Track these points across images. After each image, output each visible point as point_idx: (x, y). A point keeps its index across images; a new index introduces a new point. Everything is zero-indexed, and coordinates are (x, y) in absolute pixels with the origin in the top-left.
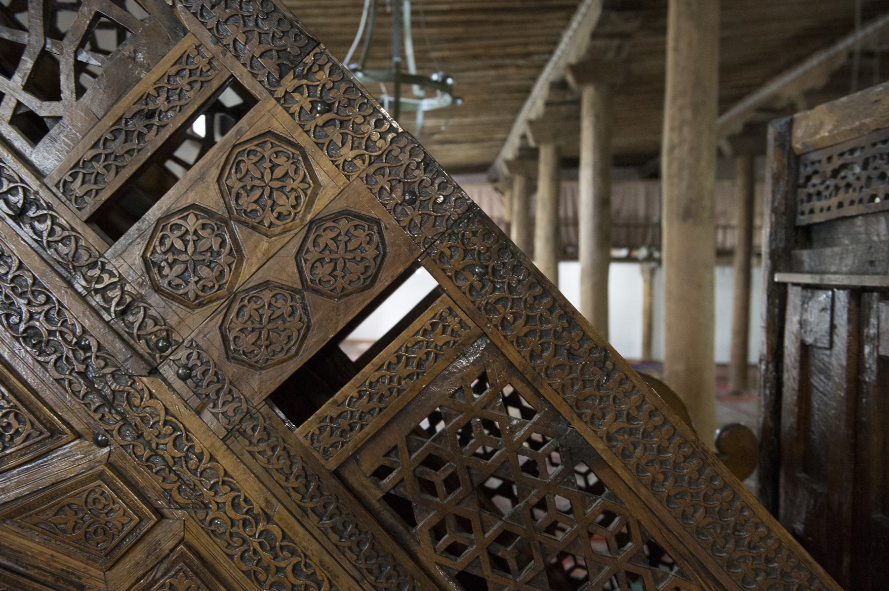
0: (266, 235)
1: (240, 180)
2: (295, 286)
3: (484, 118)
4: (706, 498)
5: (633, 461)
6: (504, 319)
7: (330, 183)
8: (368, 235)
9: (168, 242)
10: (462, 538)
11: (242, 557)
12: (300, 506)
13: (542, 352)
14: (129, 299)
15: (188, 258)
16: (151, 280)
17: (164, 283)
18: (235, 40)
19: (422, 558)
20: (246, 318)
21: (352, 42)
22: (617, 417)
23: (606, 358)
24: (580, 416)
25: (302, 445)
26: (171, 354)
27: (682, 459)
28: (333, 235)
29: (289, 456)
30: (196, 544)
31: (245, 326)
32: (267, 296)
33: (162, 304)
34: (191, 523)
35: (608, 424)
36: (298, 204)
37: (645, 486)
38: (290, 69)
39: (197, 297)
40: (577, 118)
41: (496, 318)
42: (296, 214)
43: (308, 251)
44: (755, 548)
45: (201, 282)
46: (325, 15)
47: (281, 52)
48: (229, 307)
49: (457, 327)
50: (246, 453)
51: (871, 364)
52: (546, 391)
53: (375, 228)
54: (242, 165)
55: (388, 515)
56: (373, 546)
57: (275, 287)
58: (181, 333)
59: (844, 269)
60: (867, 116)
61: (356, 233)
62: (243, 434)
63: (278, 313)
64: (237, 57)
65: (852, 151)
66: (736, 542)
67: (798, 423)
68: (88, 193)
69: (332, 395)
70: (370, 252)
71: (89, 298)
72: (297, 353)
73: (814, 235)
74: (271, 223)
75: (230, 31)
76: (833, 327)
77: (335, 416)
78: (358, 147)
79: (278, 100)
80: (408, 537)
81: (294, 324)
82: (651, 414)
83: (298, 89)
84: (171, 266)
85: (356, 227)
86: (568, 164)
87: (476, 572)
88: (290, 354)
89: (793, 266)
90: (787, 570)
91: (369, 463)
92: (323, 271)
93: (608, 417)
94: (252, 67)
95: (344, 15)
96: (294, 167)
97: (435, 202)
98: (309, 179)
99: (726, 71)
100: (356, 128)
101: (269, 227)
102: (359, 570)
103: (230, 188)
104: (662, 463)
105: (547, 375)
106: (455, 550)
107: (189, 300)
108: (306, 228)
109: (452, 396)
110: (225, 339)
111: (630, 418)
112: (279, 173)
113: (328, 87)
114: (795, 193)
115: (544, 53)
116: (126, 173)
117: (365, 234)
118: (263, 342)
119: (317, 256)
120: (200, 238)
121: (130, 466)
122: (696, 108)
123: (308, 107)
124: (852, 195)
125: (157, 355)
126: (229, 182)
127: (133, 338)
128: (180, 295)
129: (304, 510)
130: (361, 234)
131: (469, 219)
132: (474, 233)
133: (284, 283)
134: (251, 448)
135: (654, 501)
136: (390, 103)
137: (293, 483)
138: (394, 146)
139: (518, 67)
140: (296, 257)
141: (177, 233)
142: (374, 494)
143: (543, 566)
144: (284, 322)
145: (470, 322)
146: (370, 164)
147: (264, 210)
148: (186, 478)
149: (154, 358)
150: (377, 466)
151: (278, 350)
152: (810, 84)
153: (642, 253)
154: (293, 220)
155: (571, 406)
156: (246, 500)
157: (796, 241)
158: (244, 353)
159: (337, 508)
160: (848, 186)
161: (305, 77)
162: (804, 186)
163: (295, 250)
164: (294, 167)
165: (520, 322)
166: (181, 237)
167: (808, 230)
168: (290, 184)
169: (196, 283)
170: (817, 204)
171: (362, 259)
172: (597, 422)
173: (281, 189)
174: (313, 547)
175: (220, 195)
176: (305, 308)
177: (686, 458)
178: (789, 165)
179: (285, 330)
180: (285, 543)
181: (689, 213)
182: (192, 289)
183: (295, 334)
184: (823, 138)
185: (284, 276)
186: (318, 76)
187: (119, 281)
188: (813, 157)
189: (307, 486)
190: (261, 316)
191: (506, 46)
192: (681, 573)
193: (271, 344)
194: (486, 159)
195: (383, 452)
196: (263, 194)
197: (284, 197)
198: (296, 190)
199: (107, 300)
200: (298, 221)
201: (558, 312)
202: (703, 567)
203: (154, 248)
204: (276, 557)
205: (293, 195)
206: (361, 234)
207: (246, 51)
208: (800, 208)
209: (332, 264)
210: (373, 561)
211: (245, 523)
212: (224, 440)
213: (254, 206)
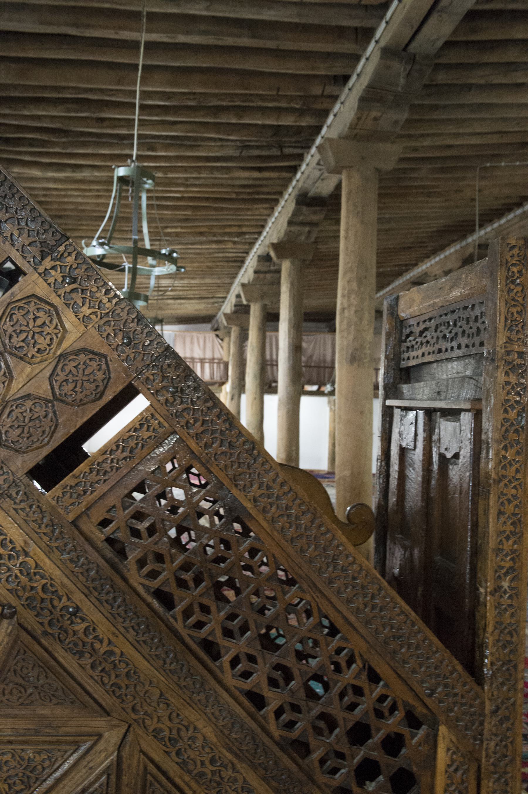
0: (29, 363)
1: (12, 326)
3: (208, 281)
5: (270, 515)
6: (188, 422)
7: (74, 331)
10: (157, 566)
11: (7, 580)
12: (48, 546)
13: (212, 443)
18: (12, 234)
19: (131, 581)
21: (104, 217)
22: (260, 486)
23: (254, 448)
24: (236, 486)
25: (50, 504)
27: (300, 514)
28: (75, 364)
29: (41, 511)
32: (29, 404)
36: (51, 343)
37: (278, 531)
38: (49, 254)
40: (278, 283)
41: (183, 422)
43: (58, 375)
44: (346, 570)
46: (84, 197)
47: (43, 243)
49: (157, 426)
50: (12, 510)
51: (435, 458)
52: (215, 470)
53: (104, 361)
54: (14, 316)
55: (108, 551)
56: (97, 572)
59: (425, 397)
60: (437, 297)
61: (91, 363)
62: (10, 496)
63: (36, 415)
64: (13, 245)
65: (430, 319)
66: (335, 567)
67: (397, 501)
69: (72, 471)
70: (100, 376)
72: (48, 442)
73: (412, 375)
76: (416, 435)
77: (73, 485)
78: (94, 307)
79: (40, 274)
80: (121, 566)
82: (282, 485)
83: (53, 268)
85: (91, 359)
86: (271, 318)
87: (166, 589)
89: (398, 395)
90: (365, 584)
91: (98, 515)
92: (67, 388)
93: (254, 487)
94: (23, 252)
95: (98, 197)
96: (49, 318)
97: (144, 345)
98: (59, 327)
99: (384, 255)
102: (87, 588)
104: (288, 516)
105: (216, 459)
106: (153, 575)
109: (153, 472)
111: (268, 487)
112: (39, 322)
113: (74, 267)
114: (400, 347)
115: (254, 233)
118: (25, 435)
122: (360, 281)
123: (60, 280)
124: (430, 349)
129: (50, 548)
130: (94, 365)
131: (166, 356)
132: (169, 366)
135: (282, 540)
136: (129, 268)
137: (44, 530)
138: (117, 307)
139: (234, 243)
142: (99, 536)
143: (256, 635)
144: (40, 421)
145: (165, 424)
146: (101, 318)
150: (101, 518)
153: (328, 388)
155: (230, 479)
156: (11, 541)
157: (401, 378)
158: (12, 442)
159: (74, 546)
160: (428, 342)
161: (58, 260)
162: (405, 341)
163: (48, 374)
164: (49, 318)
165: (199, 424)
167: (408, 369)
168: (47, 330)
170: (412, 354)
171: (95, 380)
172: (247, 490)
173: (40, 333)
174: (56, 573)
176: (54, 412)
177: (303, 513)
178: (396, 327)
180: (37, 570)
181: (354, 359)
183: (47, 430)
185: (41, 391)
186: (68, 260)
188: (411, 322)
189: (53, 532)
190: (24, 417)
191: (225, 226)
192: (300, 588)
193: (31, 436)
194: (210, 312)
195: (105, 509)
200: (51, 354)
201: (223, 418)
202: (314, 584)
204: (31, 580)
206: (94, 365)
207: (19, 241)
209: (74, 384)
210: (97, 582)
211: (10, 557)
213: (22, 344)
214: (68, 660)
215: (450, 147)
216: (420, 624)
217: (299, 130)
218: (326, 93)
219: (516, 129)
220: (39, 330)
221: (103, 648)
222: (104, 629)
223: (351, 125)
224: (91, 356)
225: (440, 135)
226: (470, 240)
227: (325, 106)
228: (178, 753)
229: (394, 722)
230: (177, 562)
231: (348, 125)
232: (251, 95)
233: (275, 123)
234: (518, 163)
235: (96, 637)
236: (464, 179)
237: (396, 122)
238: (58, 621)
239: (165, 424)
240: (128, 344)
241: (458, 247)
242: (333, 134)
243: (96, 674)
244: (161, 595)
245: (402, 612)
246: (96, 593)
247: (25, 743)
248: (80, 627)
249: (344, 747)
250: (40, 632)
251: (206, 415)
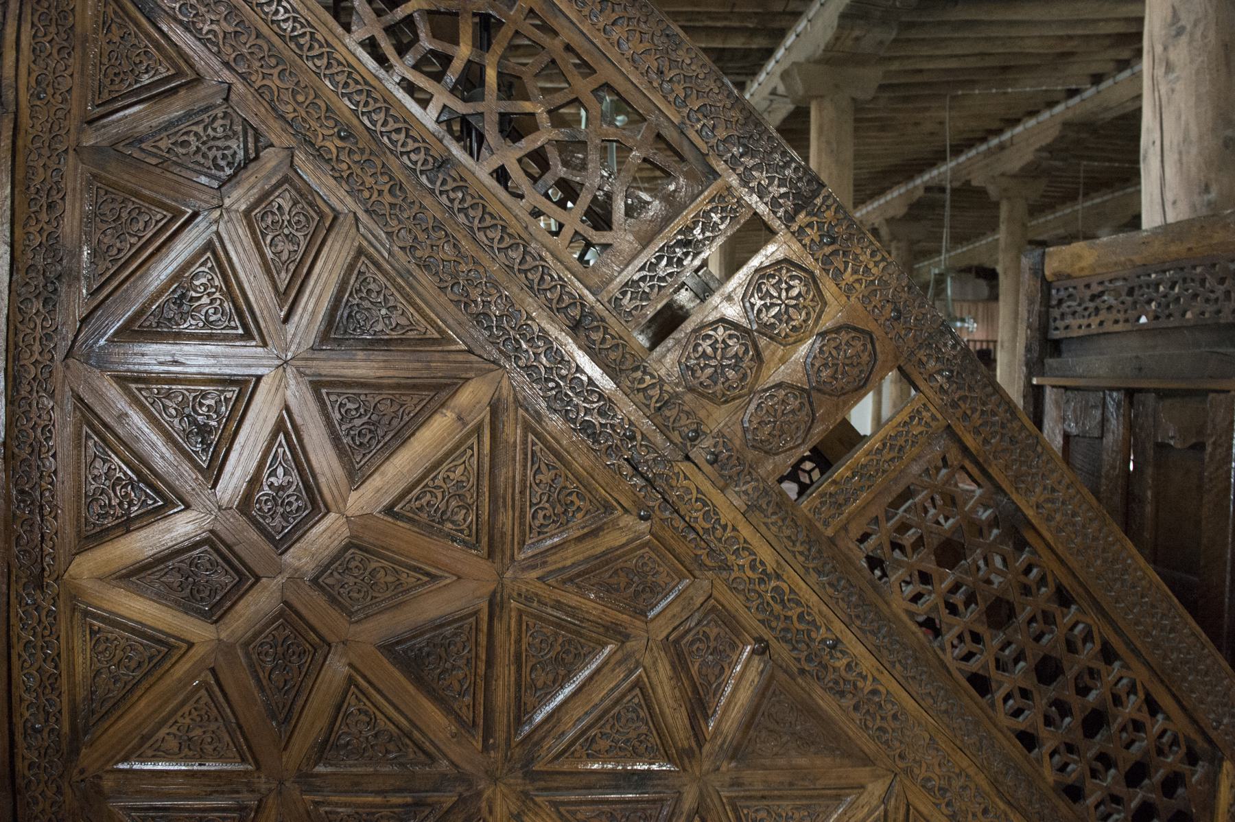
4: (1104, 550)
14: (666, 397)
25: (806, 517)
30: (722, 599)
34: (718, 582)
35: (1039, 495)
39: (724, 395)
41: (959, 413)
52: (993, 471)
62: (760, 508)
70: (865, 357)
73: (1063, 347)
75: (761, 177)
79: (793, 233)
81: (803, 415)
83: (810, 225)
84: (702, 369)
91: (855, 532)
100: (856, 257)
103: (752, 305)
121: (667, 535)
123: (817, 239)
126: (752, 300)
130: (858, 344)
134: (766, 520)
137: (799, 548)
145: (939, 416)
148: (712, 545)
149: (685, 445)
152: (891, 213)
156: (762, 563)
161: (815, 215)
170: (1069, 321)
184: (1082, 269)
189: (809, 550)
206: (858, 344)
208: (1052, 325)
212: (743, 514)
214: (826, 702)
215: (921, 71)
216: (1211, 647)
217: (746, 53)
218: (788, 9)
219: (1001, 50)
220: (794, 302)
221: (868, 686)
222: (868, 663)
223: (826, 46)
225: (909, 57)
226: (918, 181)
227: (784, 24)
228: (948, 805)
229: (1172, 760)
230: (946, 585)
231: (822, 47)
232: (699, 13)
233: (721, 46)
234: (994, 91)
235: (860, 674)
236: (927, 109)
237: (881, 43)
238: (816, 655)
239: (939, 416)
240: (897, 319)
241: (903, 190)
242: (799, 56)
243: (857, 716)
244: (928, 624)
245: (1193, 634)
246: (858, 623)
247: (780, 797)
248: (841, 663)
249: (1121, 790)
250: (795, 670)
251: (984, 404)
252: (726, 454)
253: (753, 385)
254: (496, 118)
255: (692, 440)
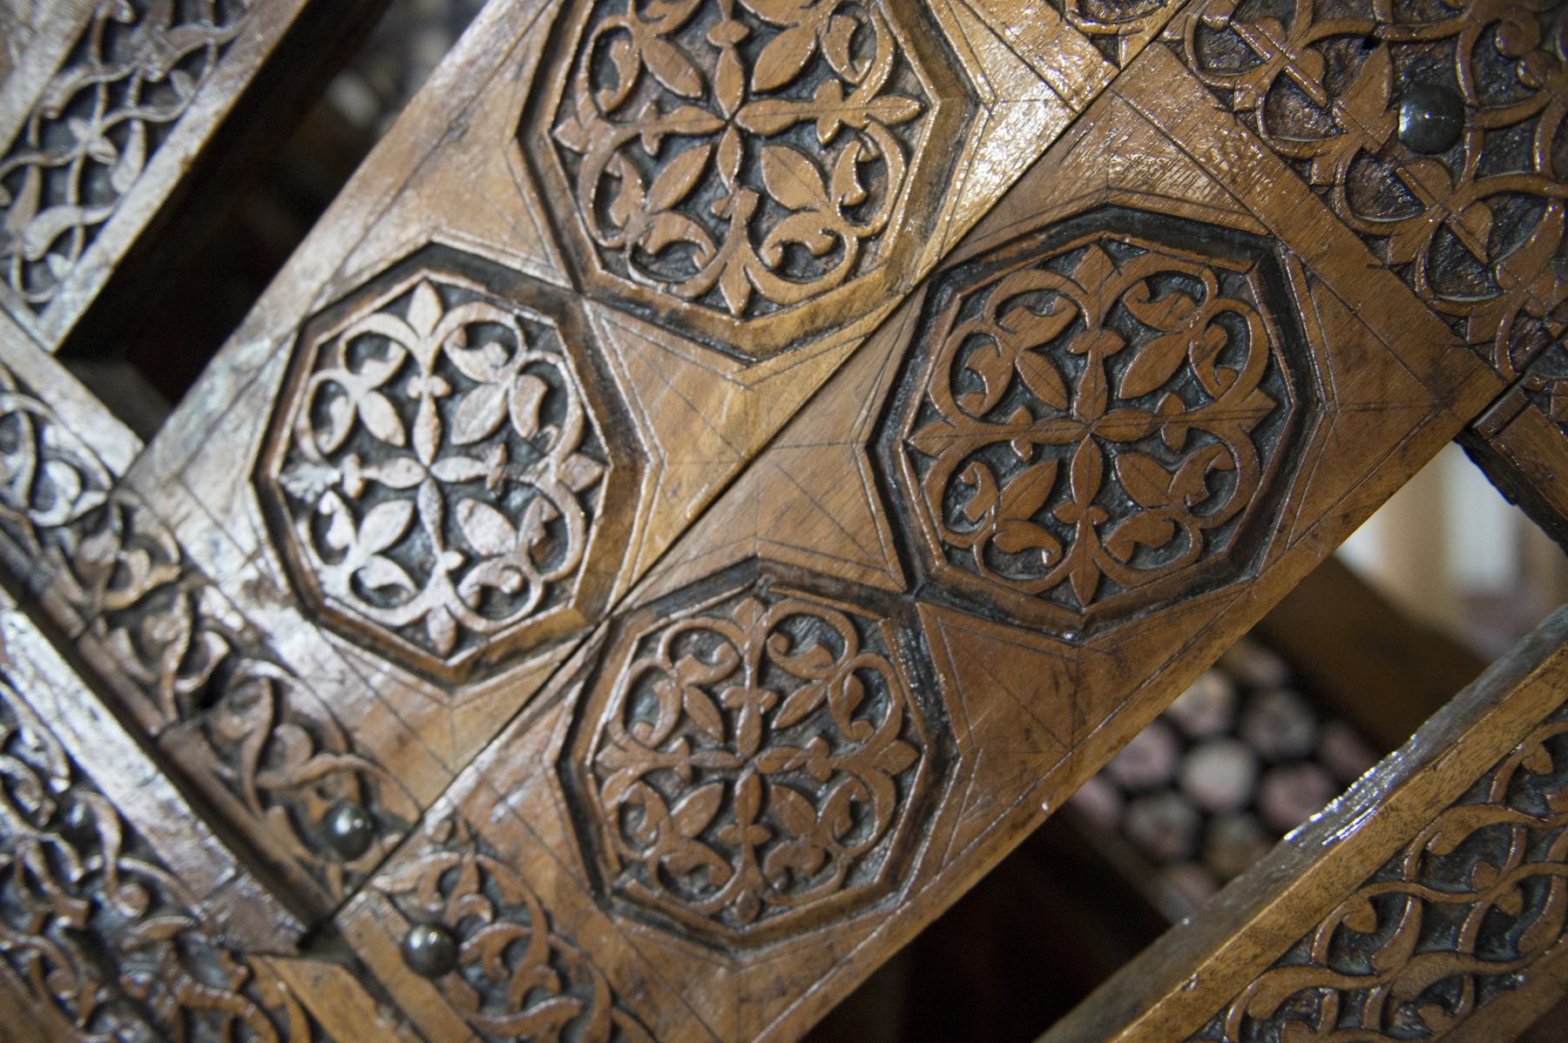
0: (731, 352)
1: (613, 115)
2: (874, 579)
8: (1214, 320)
9: (340, 413)
14: (217, 647)
15: (416, 475)
16: (290, 568)
17: (335, 580)
20: (665, 719)
26: (379, 867)
28: (1045, 331)
31: (662, 760)
33: (335, 665)
36: (869, 201)
39: (462, 635)
42: (863, 241)
45: (473, 577)
48: (592, 678)
57: (783, 583)
58: (412, 783)
61: (1154, 314)
63: (799, 700)
68: (60, 243)
70: (1235, 399)
71: (89, 646)
72: (894, 877)
73: (473, 831)
74: (753, 296)
84: (357, 509)
88: (860, 883)
101: (746, 314)
107: (432, 651)
108: (915, 309)
110: (579, 813)
112: (776, 62)
116: (185, 144)
117: (1201, 314)
119: (970, 433)
120: (458, 386)
125: (333, 872)
126: (566, 133)
127: (243, 800)
128: (399, 630)
133: (820, 565)
140: (871, 448)
141: (376, 371)
147: (718, 241)
149: (322, 880)
151: (809, 865)
154: (854, 271)
163: (861, 421)
166: (391, 388)
169: (456, 576)
171: (1192, 436)
175: (529, 195)
179: (835, 774)
182: (439, 602)
183: (882, 795)
185: (822, 536)
187: (181, 577)
190: (727, 717)
193: (776, 834)
196: (709, 167)
197: (807, 168)
198: (859, 133)
199: (145, 651)
200: (873, 274)
203: (293, 442)
205: (851, 153)
206: (1183, 325)
209: (1046, 470)
213: (677, 227)
224: (1152, 258)
252: (488, 932)
253: (599, 577)
254: (482, 472)
255: (352, 847)
